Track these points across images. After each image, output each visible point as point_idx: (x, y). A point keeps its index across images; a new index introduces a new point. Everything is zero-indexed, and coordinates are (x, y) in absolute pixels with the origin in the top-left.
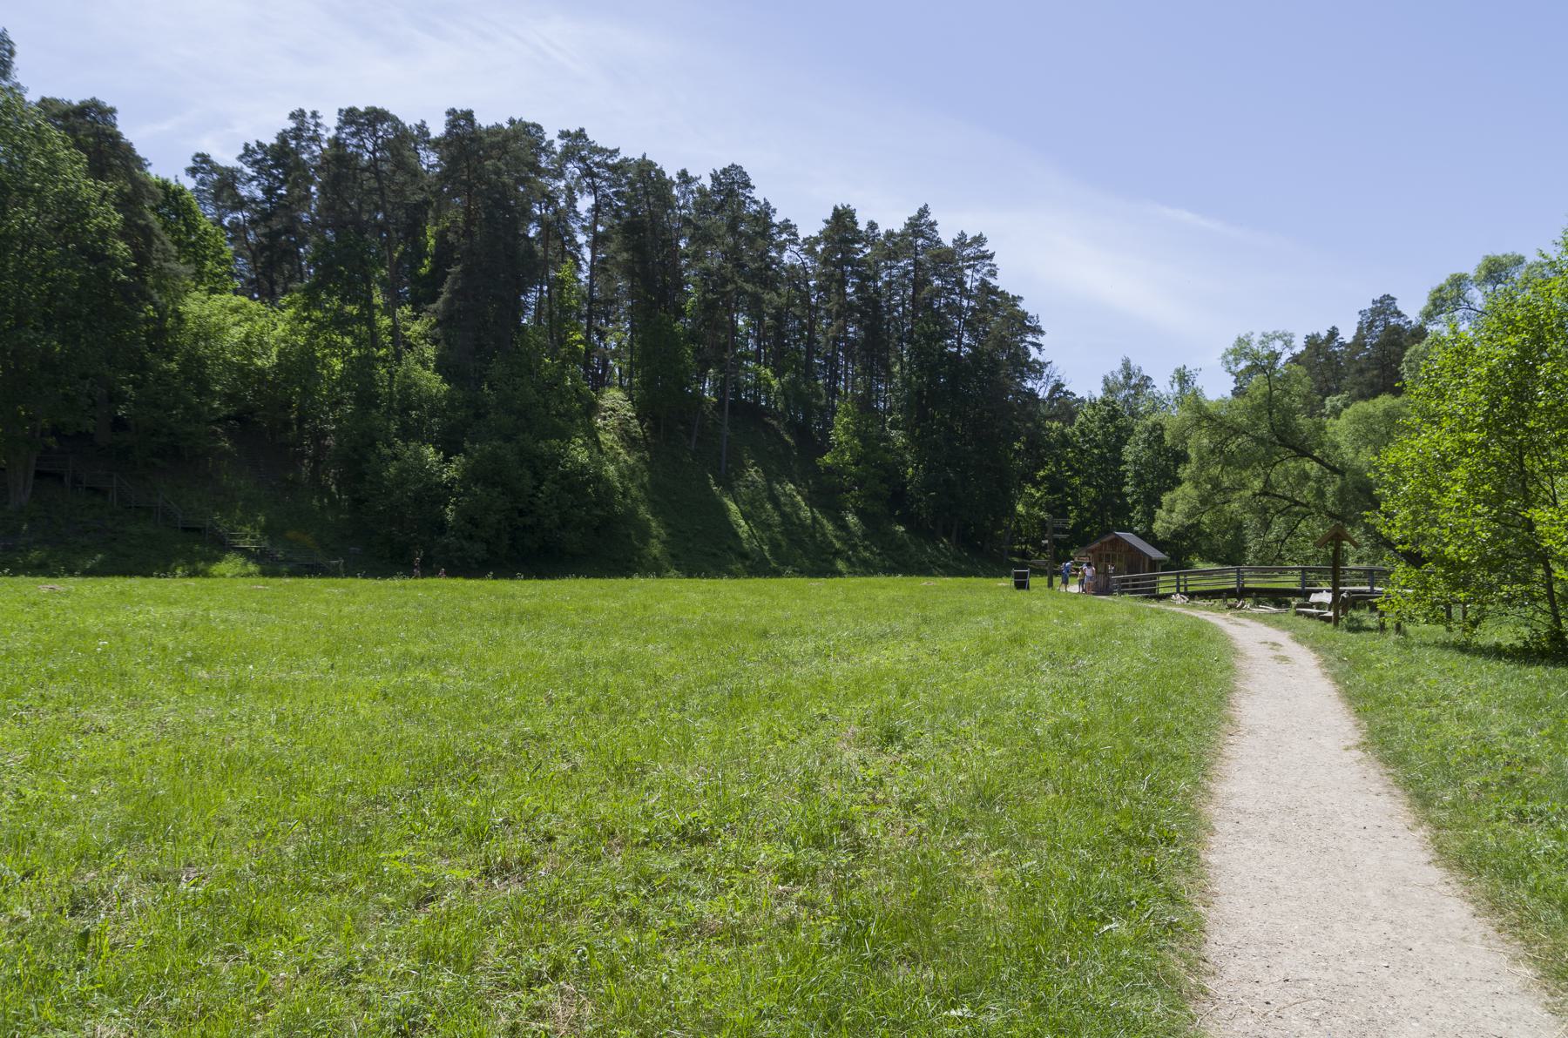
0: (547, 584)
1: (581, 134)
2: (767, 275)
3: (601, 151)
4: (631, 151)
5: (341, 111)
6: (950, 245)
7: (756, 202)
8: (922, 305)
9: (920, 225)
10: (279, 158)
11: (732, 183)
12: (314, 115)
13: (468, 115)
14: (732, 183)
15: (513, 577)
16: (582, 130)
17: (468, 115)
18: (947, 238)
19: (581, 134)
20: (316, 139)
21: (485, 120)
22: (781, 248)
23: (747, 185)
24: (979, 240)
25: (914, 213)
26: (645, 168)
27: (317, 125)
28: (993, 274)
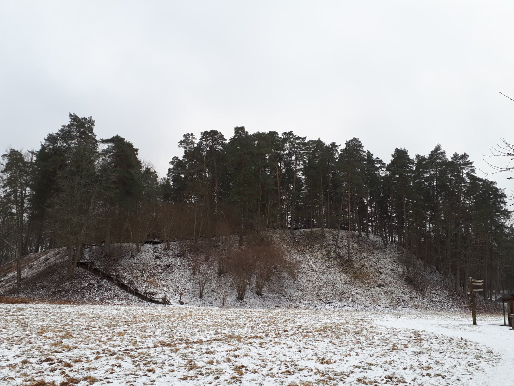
0: (68, 309)
1: (291, 133)
2: (374, 179)
3: (298, 138)
4: (311, 136)
5: (201, 133)
6: (450, 160)
7: (364, 152)
8: (442, 186)
9: (437, 153)
10: (62, 130)
11: (354, 146)
12: (192, 134)
13: (242, 128)
14: (354, 146)
15: (475, 307)
16: (291, 132)
17: (242, 128)
18: (449, 157)
19: (291, 133)
20: (192, 143)
21: (251, 131)
22: (377, 169)
23: (361, 146)
24: (465, 156)
25: (433, 149)
26: (319, 143)
27: (193, 138)
28: (473, 171)
